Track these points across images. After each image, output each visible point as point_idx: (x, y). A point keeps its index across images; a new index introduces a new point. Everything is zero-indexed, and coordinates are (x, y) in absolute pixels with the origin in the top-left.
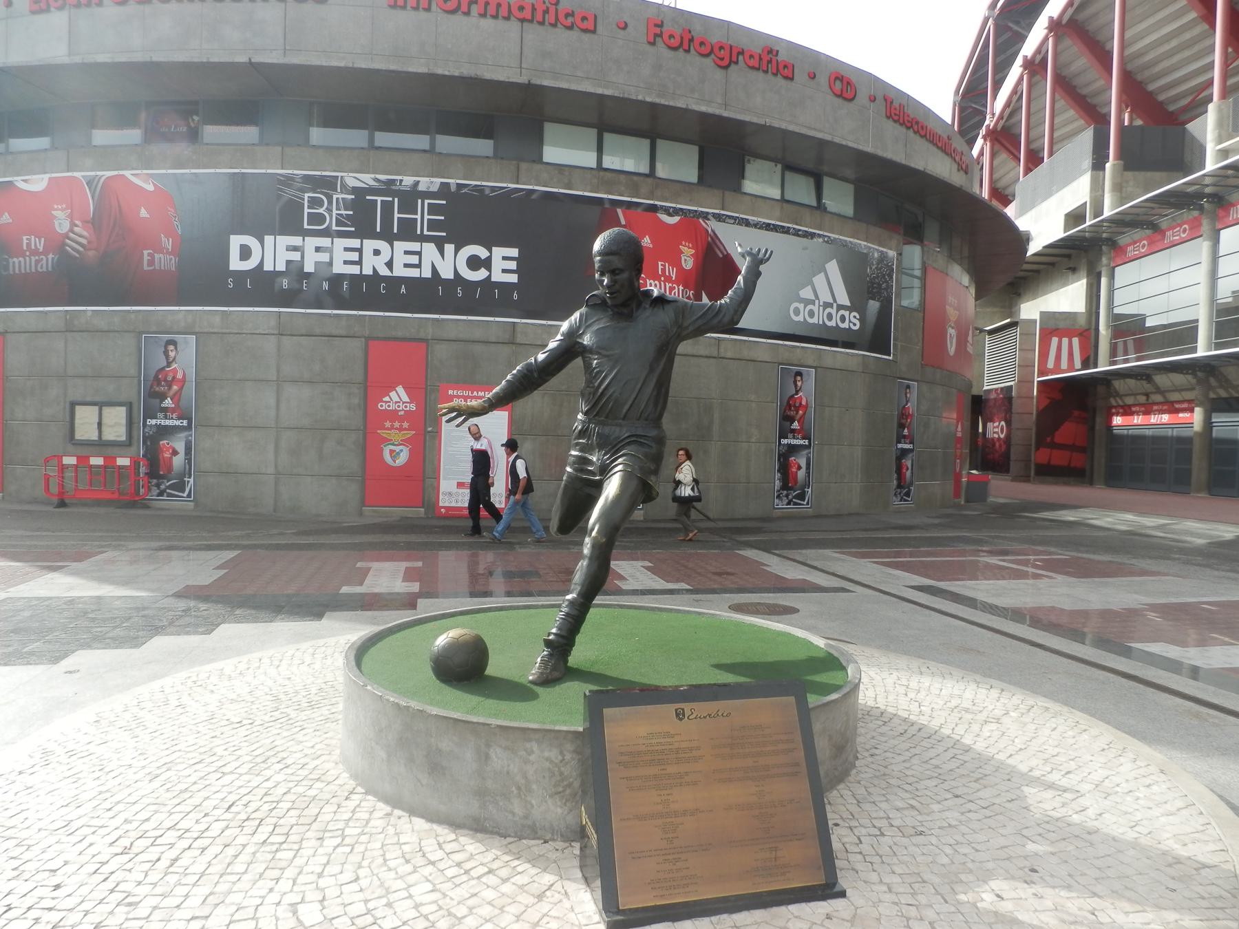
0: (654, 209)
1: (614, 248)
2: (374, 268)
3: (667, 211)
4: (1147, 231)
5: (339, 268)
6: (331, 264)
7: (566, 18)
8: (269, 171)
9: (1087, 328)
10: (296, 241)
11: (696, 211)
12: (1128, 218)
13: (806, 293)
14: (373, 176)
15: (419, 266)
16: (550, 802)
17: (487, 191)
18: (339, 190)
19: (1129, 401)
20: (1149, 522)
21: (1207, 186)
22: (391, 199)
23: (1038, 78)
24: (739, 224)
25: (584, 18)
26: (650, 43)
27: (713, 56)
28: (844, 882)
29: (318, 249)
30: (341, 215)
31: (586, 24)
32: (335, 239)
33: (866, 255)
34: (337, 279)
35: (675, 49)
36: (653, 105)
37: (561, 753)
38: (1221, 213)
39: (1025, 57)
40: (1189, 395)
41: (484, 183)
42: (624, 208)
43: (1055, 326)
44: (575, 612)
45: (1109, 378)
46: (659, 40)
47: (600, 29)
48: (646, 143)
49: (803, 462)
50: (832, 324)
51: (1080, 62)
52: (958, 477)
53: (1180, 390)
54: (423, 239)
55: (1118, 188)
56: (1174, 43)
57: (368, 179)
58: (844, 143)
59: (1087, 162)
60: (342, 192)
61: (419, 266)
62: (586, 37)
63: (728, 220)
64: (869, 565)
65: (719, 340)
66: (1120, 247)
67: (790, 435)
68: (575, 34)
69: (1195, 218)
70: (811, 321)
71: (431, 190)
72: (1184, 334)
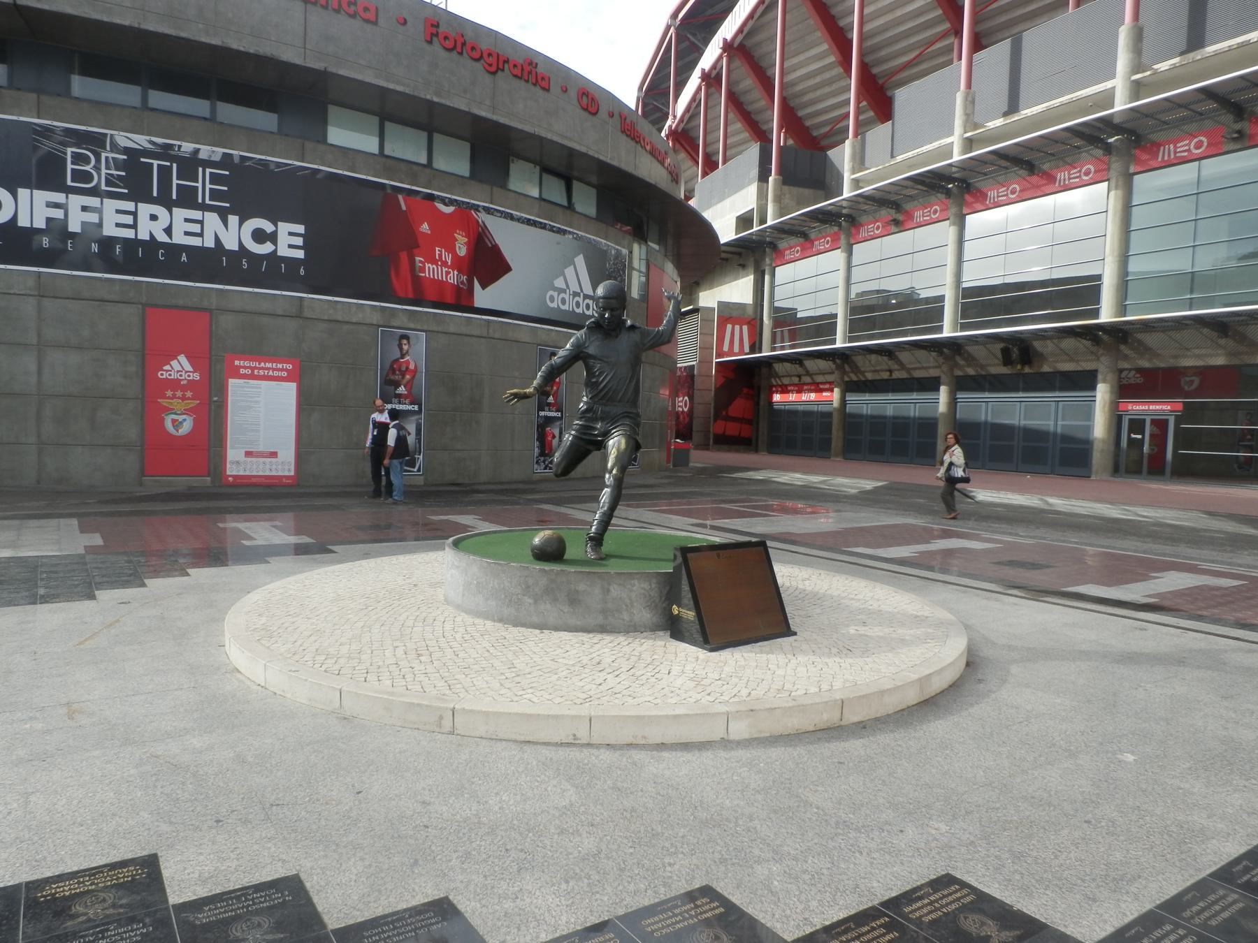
0: (431, 198)
1: (615, 295)
2: (151, 232)
3: (444, 201)
4: (800, 239)
5: (109, 230)
6: (100, 225)
7: (349, 6)
8: (22, 119)
9: (753, 317)
10: (59, 197)
11: (468, 203)
12: (787, 227)
13: (559, 283)
14: (148, 138)
15: (201, 235)
16: (643, 611)
17: (272, 167)
18: (108, 148)
19: (786, 381)
20: (814, 479)
21: (845, 208)
22: (168, 164)
23: (712, 90)
24: (505, 217)
25: (366, 9)
26: (427, 41)
27: (482, 61)
28: (793, 628)
29: (84, 209)
30: (112, 175)
31: (367, 15)
32: (104, 200)
33: (606, 252)
34: (108, 243)
35: (450, 50)
36: (431, 104)
37: (650, 585)
38: (853, 231)
39: (703, 70)
40: (830, 378)
41: (269, 158)
42: (404, 195)
43: (729, 314)
44: (605, 519)
45: (771, 361)
46: (435, 39)
47: (381, 21)
48: (424, 135)
49: (556, 432)
50: (579, 311)
51: (748, 83)
52: (669, 444)
53: (824, 374)
54: (204, 208)
55: (778, 199)
56: (818, 79)
57: (141, 141)
58: (596, 156)
59: (755, 172)
60: (112, 151)
61: (201, 235)
62: (368, 27)
63: (496, 213)
64: (647, 512)
65: (488, 321)
66: (780, 251)
67: (547, 408)
68: (357, 23)
69: (835, 233)
70: (563, 307)
71: (212, 159)
72: (824, 326)
